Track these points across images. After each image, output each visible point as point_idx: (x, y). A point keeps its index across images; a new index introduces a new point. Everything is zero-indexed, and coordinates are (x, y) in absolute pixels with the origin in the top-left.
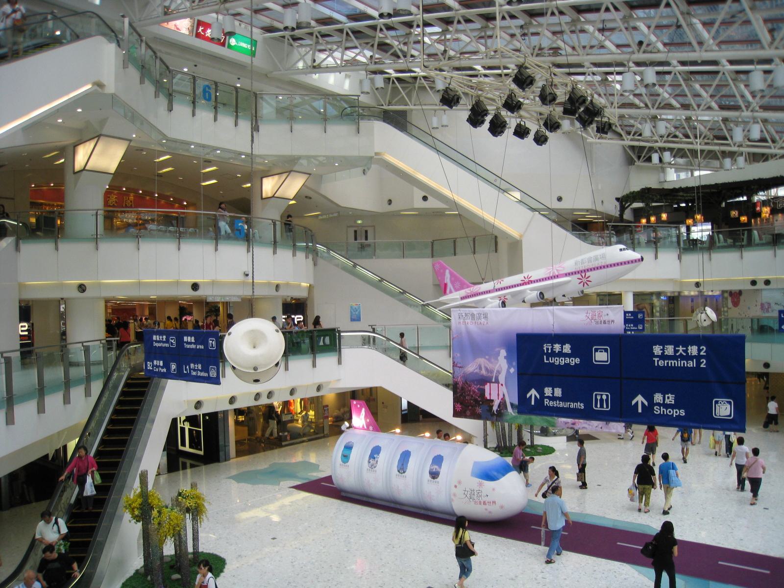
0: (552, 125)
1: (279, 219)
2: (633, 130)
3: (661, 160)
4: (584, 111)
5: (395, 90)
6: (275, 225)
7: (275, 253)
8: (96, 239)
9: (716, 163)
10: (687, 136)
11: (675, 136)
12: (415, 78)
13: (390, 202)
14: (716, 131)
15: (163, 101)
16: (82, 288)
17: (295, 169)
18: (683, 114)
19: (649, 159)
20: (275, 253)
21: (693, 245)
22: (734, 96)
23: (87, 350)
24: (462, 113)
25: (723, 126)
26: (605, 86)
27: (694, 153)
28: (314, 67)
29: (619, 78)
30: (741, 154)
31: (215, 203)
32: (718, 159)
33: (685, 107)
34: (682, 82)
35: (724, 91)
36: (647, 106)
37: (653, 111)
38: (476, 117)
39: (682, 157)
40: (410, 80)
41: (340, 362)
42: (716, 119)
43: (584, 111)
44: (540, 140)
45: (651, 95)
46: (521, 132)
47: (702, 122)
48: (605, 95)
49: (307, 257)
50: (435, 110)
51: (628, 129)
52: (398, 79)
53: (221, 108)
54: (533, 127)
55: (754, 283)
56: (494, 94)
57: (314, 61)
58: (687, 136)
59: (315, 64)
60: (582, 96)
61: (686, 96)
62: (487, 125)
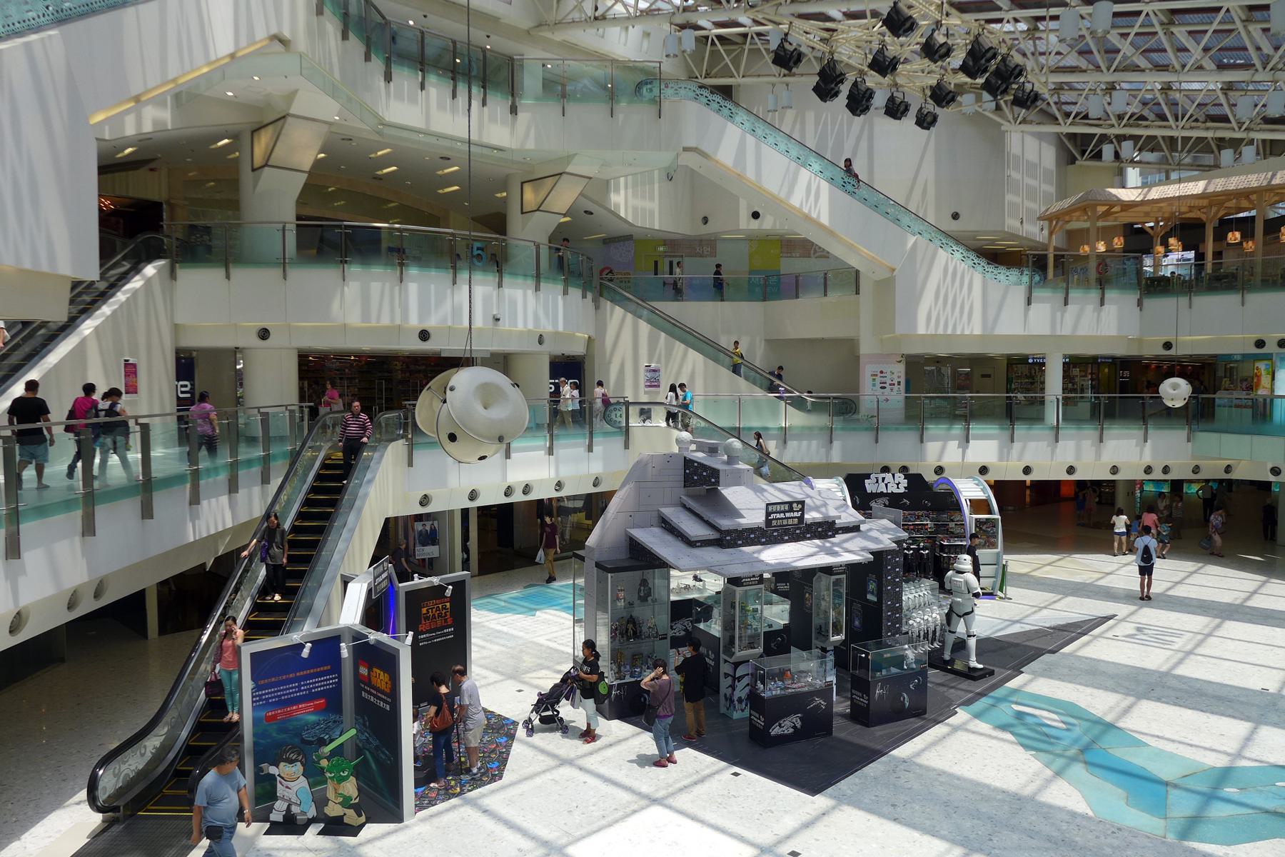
0: (942, 96)
1: (546, 241)
2: (1075, 109)
3: (1117, 156)
4: (996, 74)
5: (715, 55)
6: (538, 247)
7: (537, 289)
8: (283, 264)
9: (1208, 159)
10: (1162, 117)
11: (1145, 119)
12: (745, 36)
13: (705, 220)
14: (1209, 107)
15: (377, 64)
16: (264, 334)
17: (569, 170)
18: (1154, 81)
19: (1098, 156)
20: (537, 289)
21: (1158, 286)
22: (1245, 49)
23: (265, 418)
24: (807, 78)
25: (1223, 100)
26: (1034, 39)
27: (1172, 141)
28: (596, 18)
29: (1053, 25)
30: (1251, 142)
31: (457, 221)
32: (1213, 152)
33: (1163, 68)
34: (1158, 28)
35: (1228, 41)
36: (1098, 68)
37: (1108, 77)
38: (827, 85)
39: (1152, 150)
40: (739, 40)
41: (627, 446)
42: (1212, 87)
43: (996, 74)
44: (925, 121)
45: (1107, 52)
46: (895, 110)
47: (1190, 95)
48: (1033, 54)
49: (584, 296)
50: (774, 85)
51: (1067, 108)
52: (719, 37)
53: (459, 77)
54: (916, 100)
55: (1260, 344)
56: (853, 46)
57: (596, 9)
58: (1162, 117)
59: (597, 14)
60: (991, 48)
61: (1165, 51)
62: (842, 99)
